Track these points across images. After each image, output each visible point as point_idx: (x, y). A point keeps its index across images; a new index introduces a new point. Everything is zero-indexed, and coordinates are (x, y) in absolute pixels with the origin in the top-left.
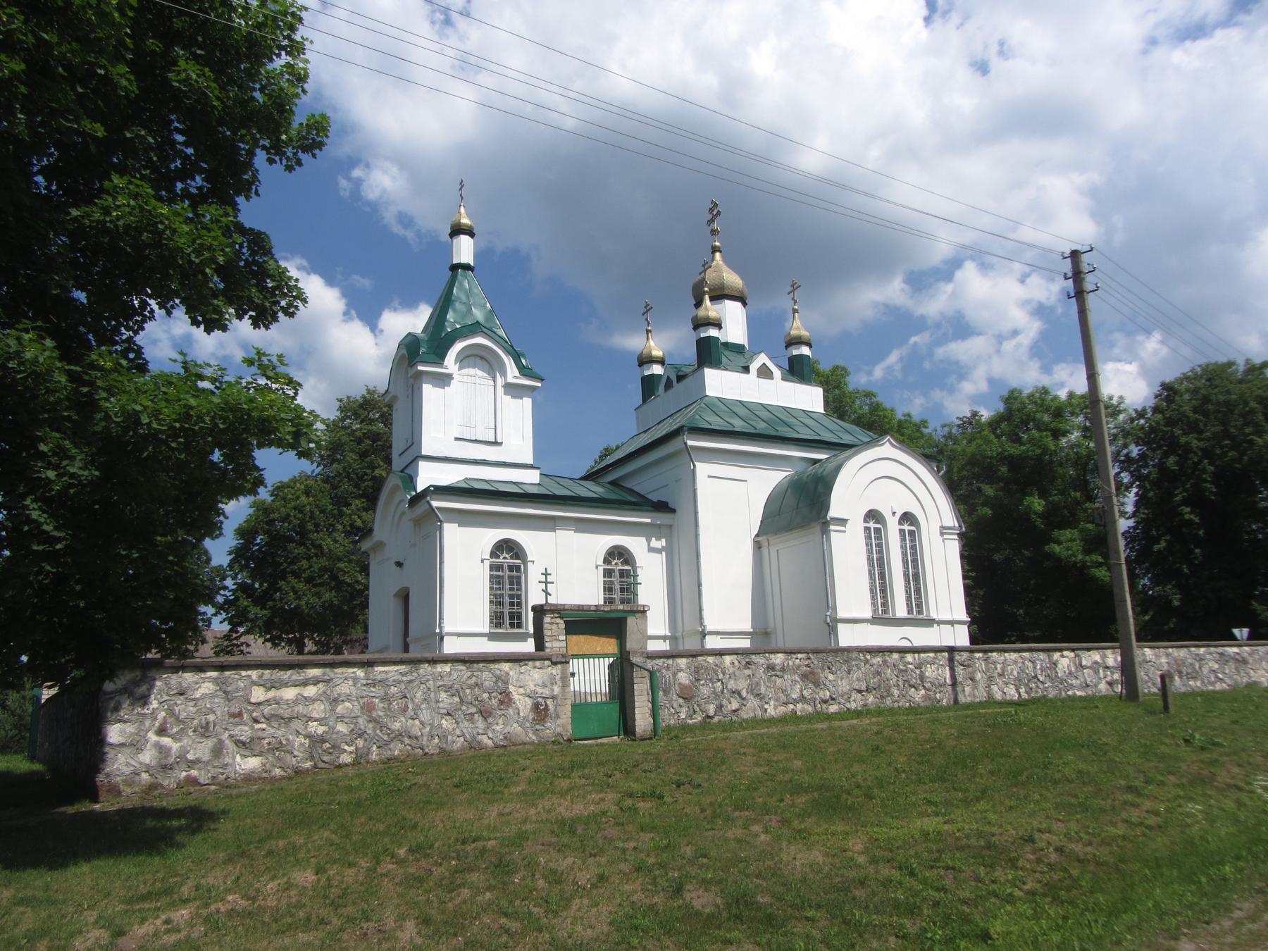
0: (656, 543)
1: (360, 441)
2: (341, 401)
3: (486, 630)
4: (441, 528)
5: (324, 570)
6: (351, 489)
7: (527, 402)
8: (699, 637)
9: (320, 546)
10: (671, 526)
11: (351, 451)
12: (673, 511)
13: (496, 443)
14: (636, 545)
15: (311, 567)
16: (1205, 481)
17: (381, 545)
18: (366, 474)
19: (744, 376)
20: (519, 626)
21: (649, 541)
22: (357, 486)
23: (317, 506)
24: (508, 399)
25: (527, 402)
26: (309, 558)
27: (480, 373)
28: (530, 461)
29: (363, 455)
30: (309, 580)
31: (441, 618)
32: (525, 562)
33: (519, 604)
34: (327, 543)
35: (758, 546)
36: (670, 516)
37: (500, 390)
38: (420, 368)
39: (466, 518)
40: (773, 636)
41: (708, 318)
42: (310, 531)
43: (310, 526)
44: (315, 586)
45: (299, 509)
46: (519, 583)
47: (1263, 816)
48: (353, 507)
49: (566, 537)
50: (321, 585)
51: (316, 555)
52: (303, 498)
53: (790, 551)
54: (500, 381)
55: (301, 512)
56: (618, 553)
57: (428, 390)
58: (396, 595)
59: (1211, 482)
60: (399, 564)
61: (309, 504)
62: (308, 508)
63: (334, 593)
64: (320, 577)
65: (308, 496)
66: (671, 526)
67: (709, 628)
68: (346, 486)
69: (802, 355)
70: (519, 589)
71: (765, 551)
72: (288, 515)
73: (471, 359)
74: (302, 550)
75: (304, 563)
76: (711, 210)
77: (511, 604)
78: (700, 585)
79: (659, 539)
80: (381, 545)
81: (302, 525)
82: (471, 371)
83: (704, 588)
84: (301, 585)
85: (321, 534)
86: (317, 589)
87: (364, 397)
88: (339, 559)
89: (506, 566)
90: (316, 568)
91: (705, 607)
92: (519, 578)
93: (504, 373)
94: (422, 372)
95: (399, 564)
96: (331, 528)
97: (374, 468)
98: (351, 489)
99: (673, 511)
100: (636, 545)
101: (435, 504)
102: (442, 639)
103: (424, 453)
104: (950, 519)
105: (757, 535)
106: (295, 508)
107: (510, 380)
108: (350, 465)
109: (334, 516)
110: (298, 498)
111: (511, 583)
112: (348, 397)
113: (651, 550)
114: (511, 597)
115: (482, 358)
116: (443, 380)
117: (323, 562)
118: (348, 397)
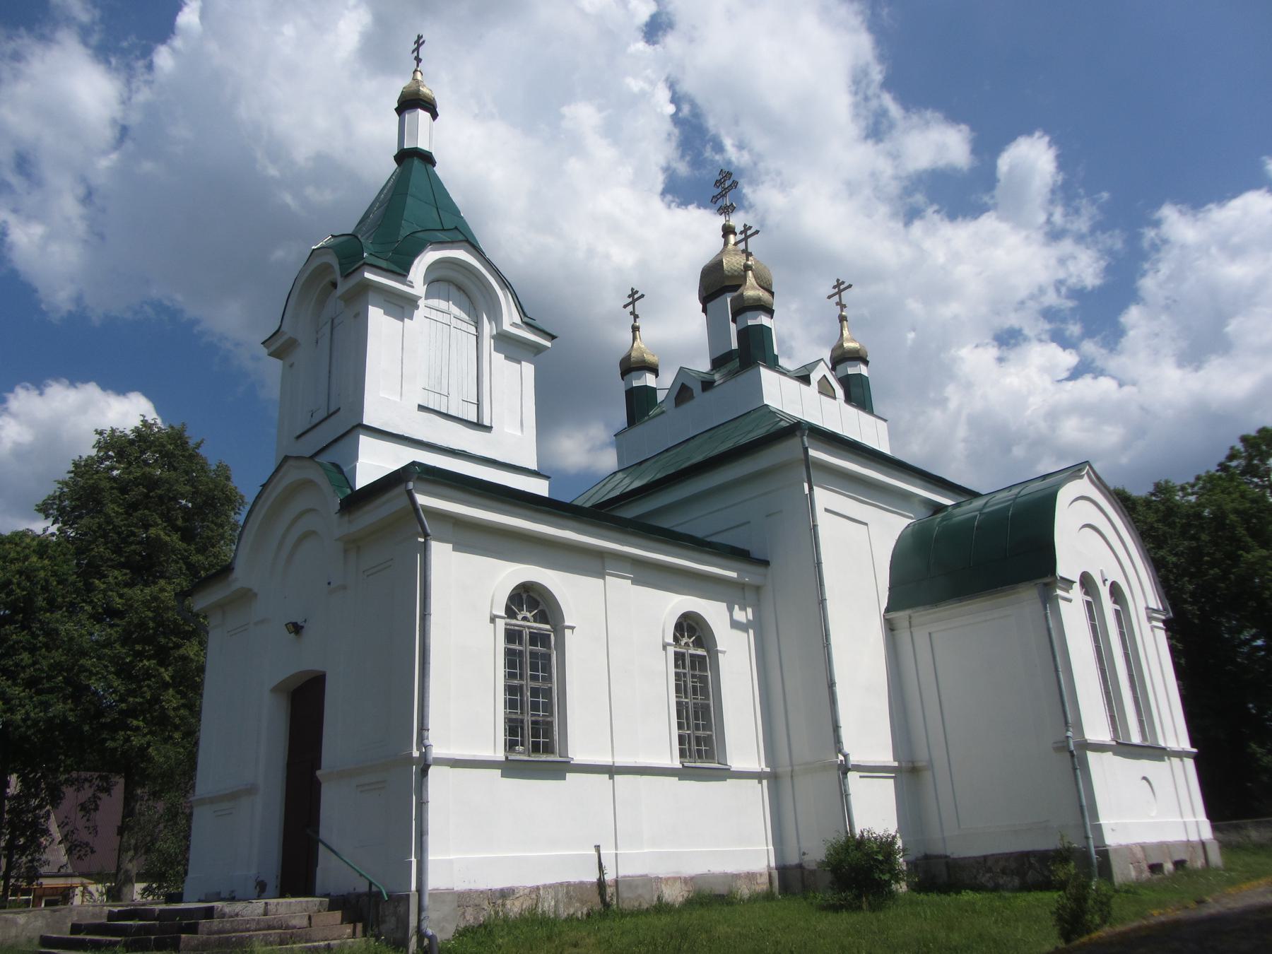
0: (740, 616)
1: (124, 490)
2: (101, 433)
3: (500, 755)
4: (425, 549)
5: (57, 667)
6: (108, 554)
7: (528, 369)
8: (835, 775)
9: (56, 631)
10: (758, 589)
11: (113, 501)
12: (765, 563)
13: (479, 426)
14: (714, 612)
15: (34, 663)
16: (1185, 601)
17: (246, 596)
18: (133, 534)
19: (803, 387)
20: (548, 749)
21: (731, 610)
22: (118, 550)
23: (55, 574)
24: (499, 358)
25: (528, 369)
26: (32, 650)
27: (455, 310)
28: (534, 466)
29: (132, 507)
30: (31, 683)
31: (423, 728)
32: (559, 627)
33: (548, 708)
34: (67, 628)
35: (890, 627)
36: (761, 570)
37: (488, 343)
38: (367, 275)
39: (473, 537)
40: (927, 775)
41: (644, 361)
42: (41, 609)
43: (40, 601)
44: (39, 692)
45: (28, 574)
46: (547, 668)
47: (855, 951)
48: (111, 579)
49: (620, 588)
50: (51, 691)
51: (46, 646)
52: (34, 559)
53: (969, 632)
54: (488, 328)
55: (28, 578)
56: (690, 626)
57: (376, 317)
58: (276, 689)
59: (1192, 604)
60: (296, 629)
61: (43, 568)
62: (42, 574)
63: (70, 704)
64: (50, 678)
65: (41, 557)
66: (758, 589)
67: (854, 759)
68: (100, 549)
69: (860, 375)
70: (548, 679)
71: (904, 636)
72: (9, 582)
73: (443, 286)
74: (24, 636)
75: (25, 657)
76: (718, 183)
77: (535, 706)
78: (831, 685)
79: (743, 608)
80: (246, 596)
81: (29, 600)
82: (442, 304)
83: (839, 689)
84: (17, 690)
85: (58, 615)
86: (44, 698)
87: (136, 430)
88: (83, 654)
89: (526, 633)
90: (44, 664)
91: (843, 722)
92: (548, 657)
93: (496, 316)
94: (369, 285)
95: (296, 629)
96: (72, 609)
97: (146, 527)
98: (108, 554)
99: (765, 563)
100: (714, 612)
101: (422, 499)
102: (424, 772)
103: (365, 422)
104: (1154, 602)
105: (888, 610)
106: (20, 573)
107: (507, 327)
108: (109, 522)
109: (77, 591)
110: (26, 558)
111: (534, 667)
112: (113, 430)
113: (735, 625)
114: (535, 692)
115: (460, 288)
116: (402, 306)
117: (58, 656)
118: (113, 430)
